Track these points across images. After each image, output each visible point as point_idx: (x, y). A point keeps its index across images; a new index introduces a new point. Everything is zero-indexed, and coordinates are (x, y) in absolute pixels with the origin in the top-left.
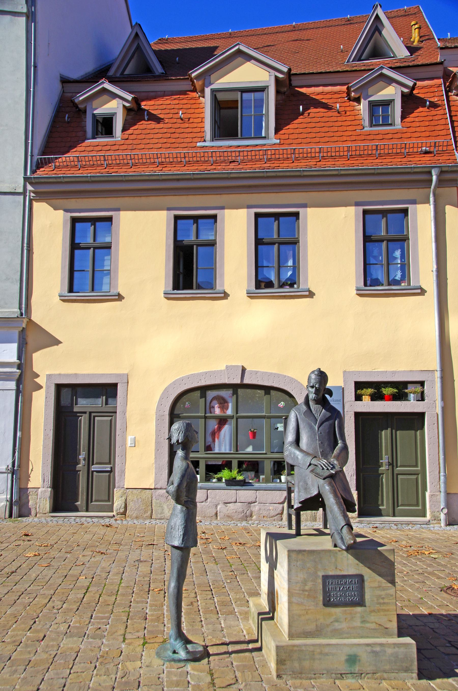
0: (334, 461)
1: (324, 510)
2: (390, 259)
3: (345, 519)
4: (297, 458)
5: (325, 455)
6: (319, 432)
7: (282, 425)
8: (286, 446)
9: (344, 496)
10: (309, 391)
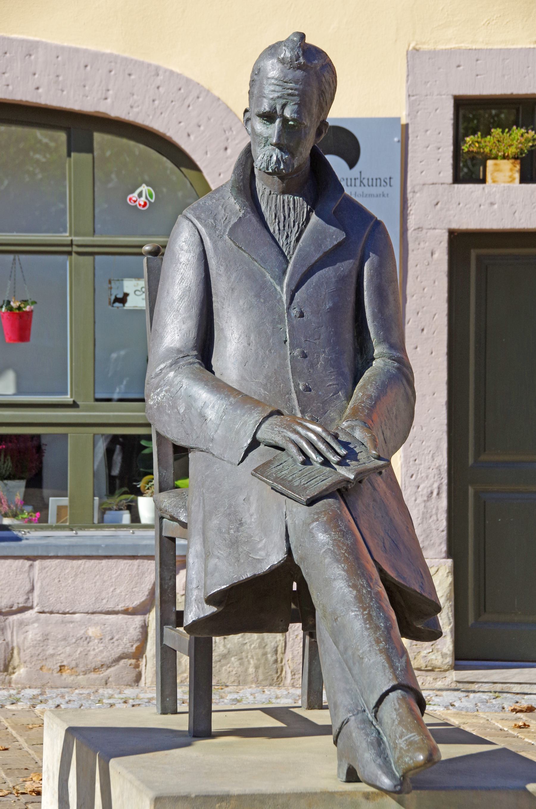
0: (352, 428)
1: (310, 630)
3: (392, 666)
4: (203, 417)
5: (314, 405)
6: (294, 312)
7: (142, 283)
8: (157, 367)
9: (392, 574)
10: (254, 133)
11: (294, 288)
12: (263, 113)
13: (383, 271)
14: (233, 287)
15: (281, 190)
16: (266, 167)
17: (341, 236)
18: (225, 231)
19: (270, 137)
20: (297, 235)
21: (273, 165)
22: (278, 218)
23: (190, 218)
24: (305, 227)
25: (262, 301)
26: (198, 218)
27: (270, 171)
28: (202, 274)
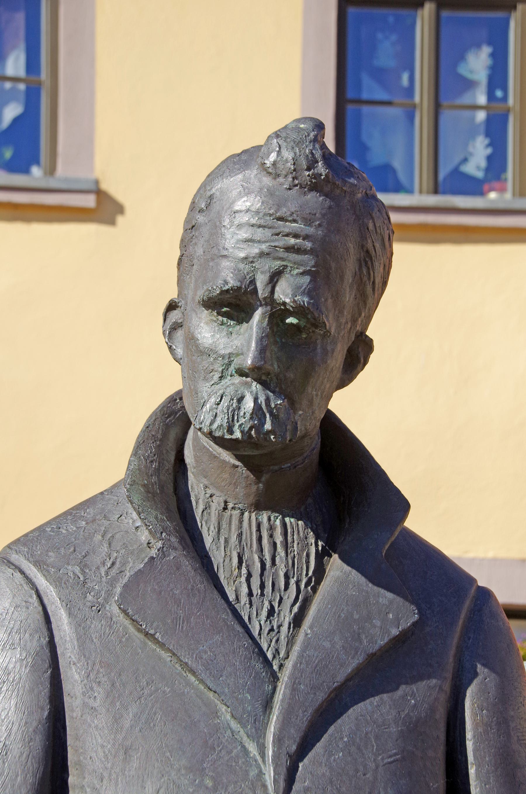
2: (445, 84)
11: (294, 748)
12: (222, 292)
13: (512, 713)
14: (128, 743)
15: (252, 499)
16: (225, 425)
17: (409, 615)
18: (109, 594)
19: (237, 355)
20: (296, 609)
21: (244, 420)
22: (248, 566)
23: (17, 563)
24: (315, 590)
25: (209, 783)
26: (38, 564)
27: (238, 435)
28: (42, 709)
